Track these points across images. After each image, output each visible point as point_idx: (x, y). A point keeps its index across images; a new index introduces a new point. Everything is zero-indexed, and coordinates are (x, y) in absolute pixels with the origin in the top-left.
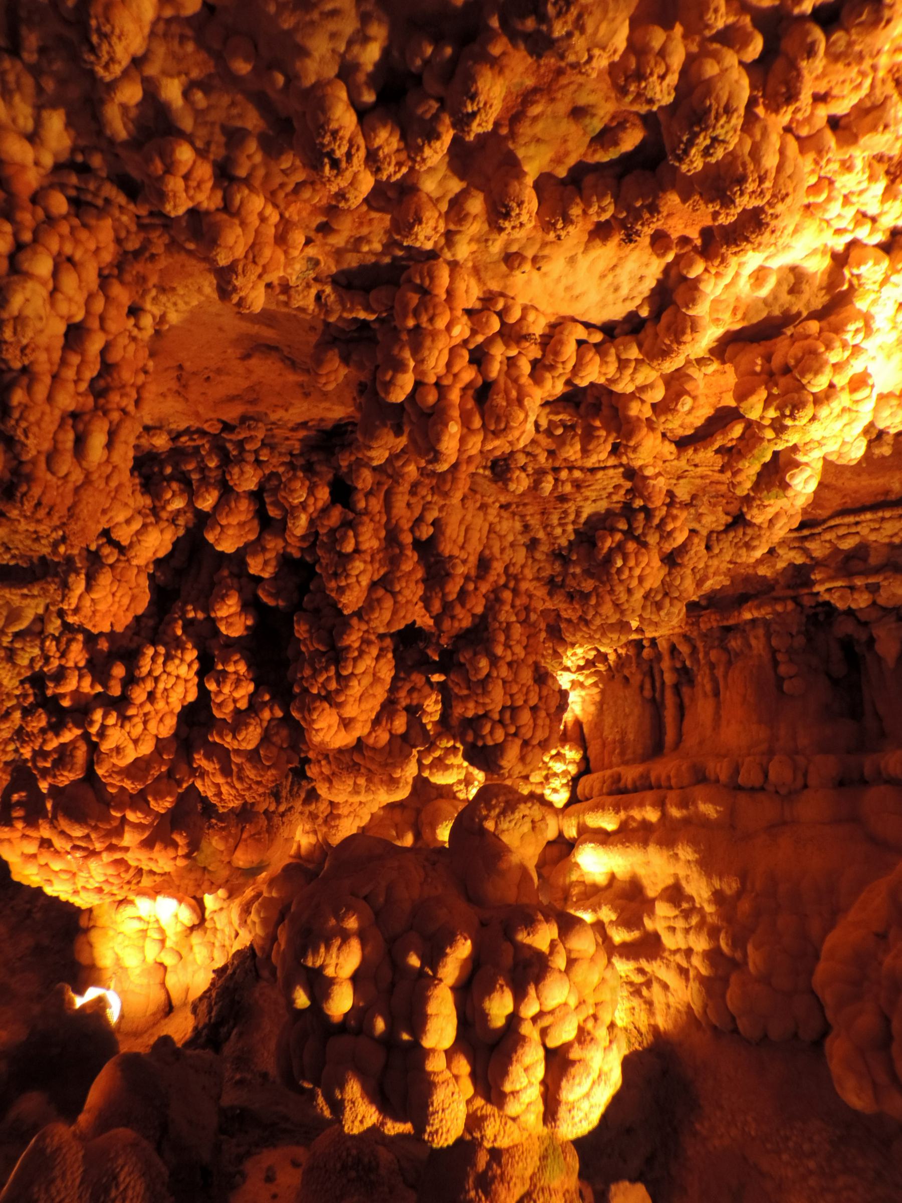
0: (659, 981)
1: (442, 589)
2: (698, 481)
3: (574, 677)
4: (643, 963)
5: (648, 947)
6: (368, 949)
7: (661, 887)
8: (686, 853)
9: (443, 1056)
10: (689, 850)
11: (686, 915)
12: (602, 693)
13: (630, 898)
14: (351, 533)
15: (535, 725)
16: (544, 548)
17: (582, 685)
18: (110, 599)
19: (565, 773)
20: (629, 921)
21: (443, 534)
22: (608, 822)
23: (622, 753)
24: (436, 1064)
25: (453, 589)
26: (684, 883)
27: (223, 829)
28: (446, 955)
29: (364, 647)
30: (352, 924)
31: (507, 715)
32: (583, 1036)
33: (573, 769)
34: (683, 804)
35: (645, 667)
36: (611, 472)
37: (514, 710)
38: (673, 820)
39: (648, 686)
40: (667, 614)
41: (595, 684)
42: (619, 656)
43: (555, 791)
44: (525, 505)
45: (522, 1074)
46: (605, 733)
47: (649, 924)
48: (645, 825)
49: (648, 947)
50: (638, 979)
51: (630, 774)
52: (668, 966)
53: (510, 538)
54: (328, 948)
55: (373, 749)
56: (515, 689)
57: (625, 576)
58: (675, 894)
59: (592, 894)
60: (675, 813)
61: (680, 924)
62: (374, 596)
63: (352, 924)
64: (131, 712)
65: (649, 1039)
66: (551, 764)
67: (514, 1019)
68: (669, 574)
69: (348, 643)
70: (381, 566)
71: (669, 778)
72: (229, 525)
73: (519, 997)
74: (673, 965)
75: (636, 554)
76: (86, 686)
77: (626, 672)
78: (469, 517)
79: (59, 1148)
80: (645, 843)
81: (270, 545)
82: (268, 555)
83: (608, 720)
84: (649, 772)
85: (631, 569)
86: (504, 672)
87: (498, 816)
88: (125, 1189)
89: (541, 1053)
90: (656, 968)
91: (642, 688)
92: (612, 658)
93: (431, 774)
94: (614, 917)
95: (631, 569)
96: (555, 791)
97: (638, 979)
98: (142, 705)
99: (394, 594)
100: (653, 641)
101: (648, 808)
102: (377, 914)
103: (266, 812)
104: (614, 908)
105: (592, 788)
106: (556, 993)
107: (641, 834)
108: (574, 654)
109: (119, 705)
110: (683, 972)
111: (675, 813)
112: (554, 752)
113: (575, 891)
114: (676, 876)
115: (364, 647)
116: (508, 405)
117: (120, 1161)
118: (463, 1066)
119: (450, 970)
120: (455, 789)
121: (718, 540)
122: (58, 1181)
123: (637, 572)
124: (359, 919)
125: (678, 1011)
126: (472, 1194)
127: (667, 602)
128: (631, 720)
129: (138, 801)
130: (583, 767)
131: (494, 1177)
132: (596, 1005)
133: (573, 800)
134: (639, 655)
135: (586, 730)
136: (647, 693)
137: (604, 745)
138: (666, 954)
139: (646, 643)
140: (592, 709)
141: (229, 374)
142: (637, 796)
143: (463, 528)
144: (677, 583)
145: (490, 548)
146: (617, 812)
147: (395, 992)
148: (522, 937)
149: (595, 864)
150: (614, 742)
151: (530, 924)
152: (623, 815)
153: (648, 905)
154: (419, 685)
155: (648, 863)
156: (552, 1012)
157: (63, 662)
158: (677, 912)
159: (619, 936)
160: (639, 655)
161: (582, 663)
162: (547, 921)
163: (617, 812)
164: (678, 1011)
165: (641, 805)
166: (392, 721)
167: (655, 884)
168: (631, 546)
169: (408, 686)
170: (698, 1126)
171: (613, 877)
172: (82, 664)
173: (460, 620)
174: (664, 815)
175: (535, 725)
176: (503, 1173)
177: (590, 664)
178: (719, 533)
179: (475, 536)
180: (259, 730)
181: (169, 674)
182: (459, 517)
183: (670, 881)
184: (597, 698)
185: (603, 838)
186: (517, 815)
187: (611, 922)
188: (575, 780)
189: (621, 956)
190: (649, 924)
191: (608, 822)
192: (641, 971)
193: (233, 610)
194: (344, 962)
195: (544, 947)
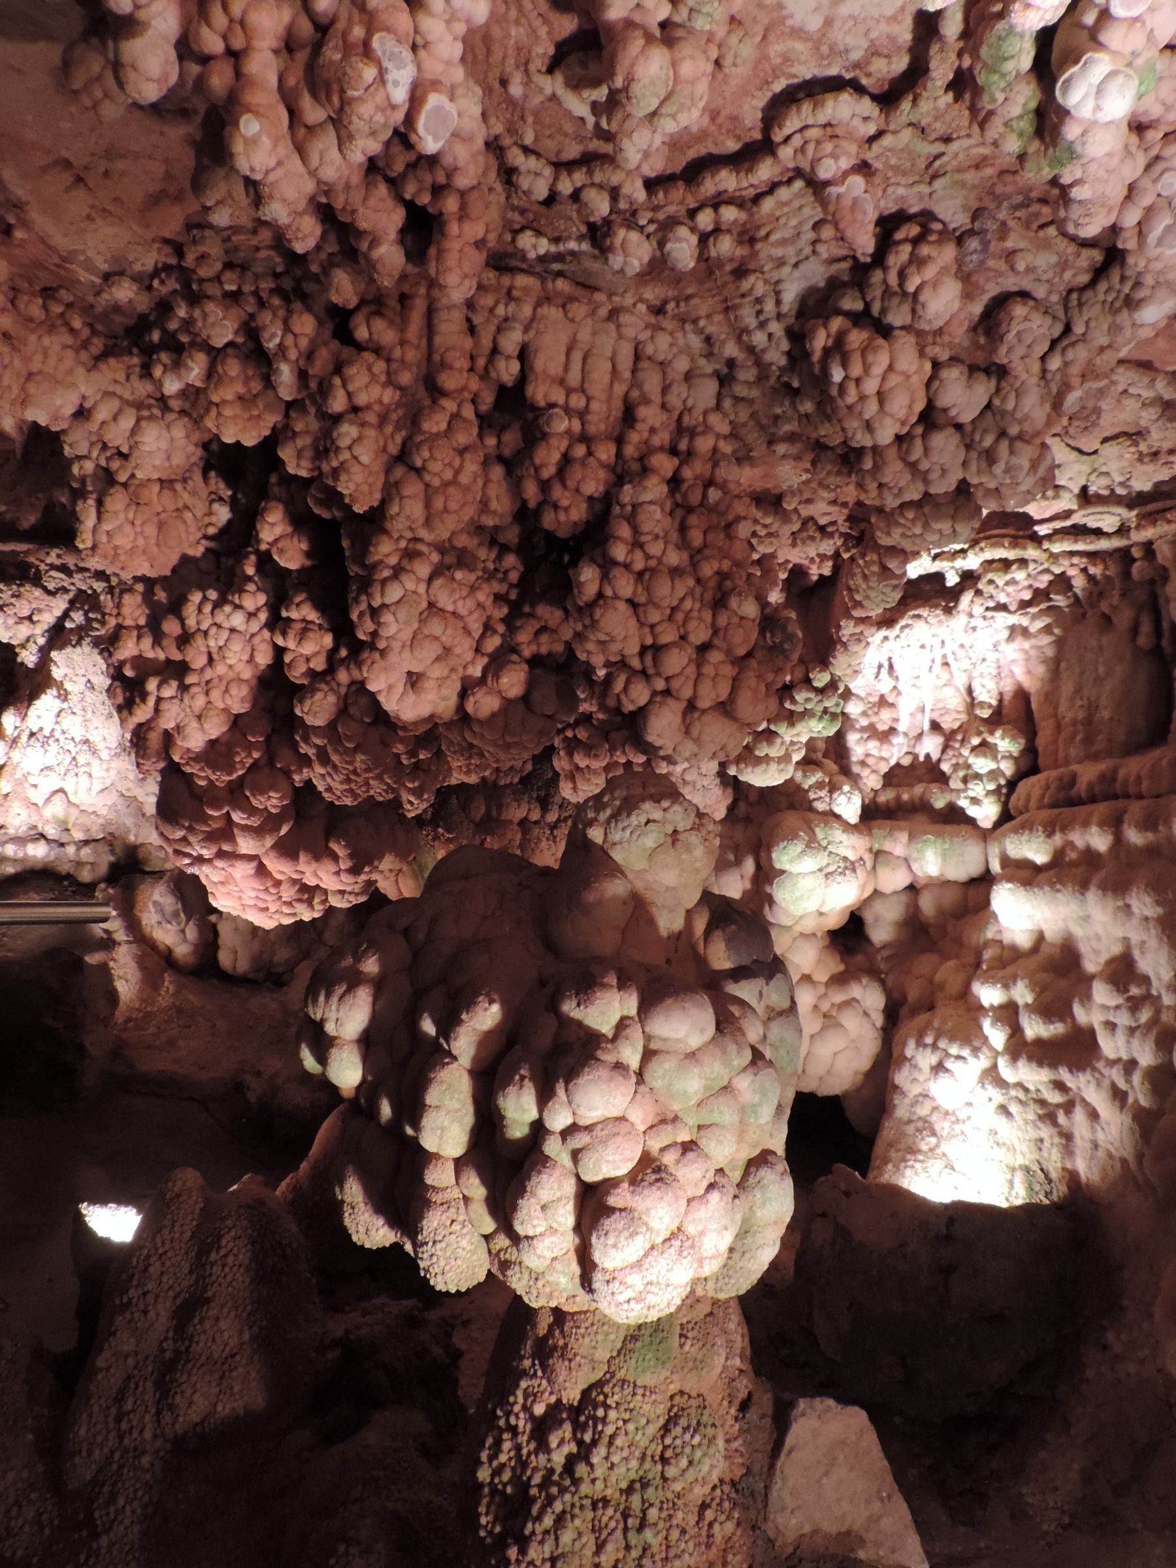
0: (1086, 1104)
1: (532, 459)
2: (971, 177)
3: (1013, 619)
4: (1064, 1075)
5: (1076, 1049)
6: (381, 1003)
7: (1105, 957)
8: (1143, 905)
9: (451, 1166)
10: (1148, 900)
11: (1134, 1005)
12: (1060, 643)
13: (1058, 971)
14: (337, 381)
15: (699, 675)
16: (747, 374)
17: (1025, 632)
18: (128, 529)
19: (994, 774)
20: (1049, 1009)
21: (532, 369)
22: (1036, 850)
23: (1088, 740)
24: (439, 1176)
25: (548, 457)
26: (1136, 954)
27: (449, 840)
28: (460, 1022)
29: (405, 563)
30: (371, 966)
31: (649, 658)
32: (648, 1170)
33: (1007, 768)
34: (1148, 823)
35: (1141, 595)
36: (784, 193)
37: (654, 650)
38: (1131, 850)
39: (1146, 627)
40: (1007, 471)
41: (1047, 629)
42: (1091, 578)
43: (975, 801)
44: (688, 298)
45: (539, 1213)
46: (1062, 708)
47: (1081, 1015)
48: (1090, 857)
49: (1076, 1049)
50: (1055, 1098)
51: (1088, 773)
52: (1099, 1084)
53: (682, 365)
54: (328, 997)
55: (479, 720)
56: (654, 616)
57: (852, 396)
58: (1122, 971)
59: (1008, 961)
60: (1134, 837)
61: (1123, 1019)
62: (392, 480)
63: (371, 966)
64: (190, 679)
65: (1060, 1191)
66: (971, 760)
67: (538, 1129)
68: (998, 390)
69: (376, 558)
70: (398, 428)
71: (1139, 779)
72: (224, 401)
73: (544, 1097)
74: (1107, 1082)
75: (864, 352)
76: (147, 648)
77: (1104, 606)
78: (584, 336)
79: (178, 1196)
80: (1083, 886)
81: (299, 427)
82: (300, 442)
83: (1067, 687)
84: (1115, 770)
85: (858, 381)
86: (625, 585)
87: (608, 822)
88: (225, 1256)
89: (569, 1188)
90: (1085, 1085)
91: (1135, 631)
92: (1079, 583)
93: (739, 770)
94: (1030, 1000)
95: (858, 381)
96: (975, 801)
97: (1055, 1098)
98: (202, 670)
99: (418, 471)
100: (1148, 546)
101: (1094, 829)
102: (416, 955)
103: (523, 822)
104: (1032, 986)
105: (1028, 799)
106: (597, 1098)
107: (1077, 871)
108: (1013, 582)
109: (177, 671)
110: (1118, 1096)
111: (1134, 837)
112: (976, 741)
113: (987, 955)
114: (1126, 941)
115: (405, 563)
116: (346, 57)
117: (229, 1223)
118: (476, 1188)
119: (464, 1044)
120: (812, 796)
121: (1080, 305)
122: (166, 1232)
123: (871, 386)
124: (381, 961)
125: (1110, 1156)
126: (527, 1363)
127: (1004, 446)
128: (1108, 686)
129: (235, 794)
130: (1025, 764)
131: (555, 1347)
132: (700, 1127)
133: (1005, 817)
134: (1126, 574)
135: (1034, 706)
136: (1144, 641)
137: (1058, 727)
138: (1100, 1065)
139: (1136, 553)
140: (1040, 670)
141: (122, 157)
142: (1083, 810)
143: (577, 356)
144: (1010, 405)
145: (639, 386)
146: (1050, 835)
147: (401, 1063)
148: (569, 1008)
149: (1017, 915)
150: (1074, 722)
151: (586, 985)
152: (1058, 839)
153: (1081, 983)
154: (552, 623)
155: (1087, 919)
156: (589, 1128)
157: (120, 620)
158: (1120, 1000)
159: (1034, 1028)
160: (1126, 574)
161: (1027, 595)
162: (621, 986)
163: (1050, 835)
164: (1110, 1156)
165: (1086, 824)
166: (498, 678)
167: (1096, 952)
168: (856, 338)
169: (534, 625)
170: (1110, 1336)
171: (1040, 938)
172: (142, 621)
173: (566, 509)
174: (1118, 839)
175: (699, 675)
176: (566, 1345)
177: (1040, 595)
178: (1082, 289)
179: (601, 370)
180: (332, 699)
181: (219, 626)
182: (564, 338)
183: (1117, 949)
184: (1050, 652)
185: (1026, 874)
186: (637, 819)
187: (1027, 1005)
188: (1012, 784)
189: (1030, 1059)
190: (1081, 1015)
191: (1036, 850)
192: (1059, 1086)
193: (278, 530)
194: (349, 1017)
195: (606, 1027)
